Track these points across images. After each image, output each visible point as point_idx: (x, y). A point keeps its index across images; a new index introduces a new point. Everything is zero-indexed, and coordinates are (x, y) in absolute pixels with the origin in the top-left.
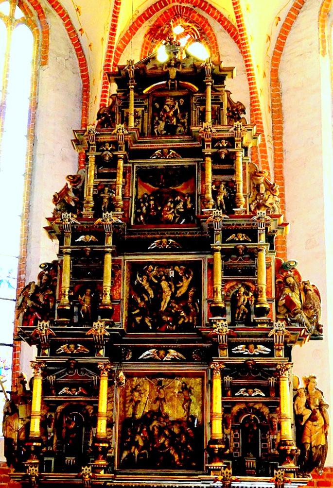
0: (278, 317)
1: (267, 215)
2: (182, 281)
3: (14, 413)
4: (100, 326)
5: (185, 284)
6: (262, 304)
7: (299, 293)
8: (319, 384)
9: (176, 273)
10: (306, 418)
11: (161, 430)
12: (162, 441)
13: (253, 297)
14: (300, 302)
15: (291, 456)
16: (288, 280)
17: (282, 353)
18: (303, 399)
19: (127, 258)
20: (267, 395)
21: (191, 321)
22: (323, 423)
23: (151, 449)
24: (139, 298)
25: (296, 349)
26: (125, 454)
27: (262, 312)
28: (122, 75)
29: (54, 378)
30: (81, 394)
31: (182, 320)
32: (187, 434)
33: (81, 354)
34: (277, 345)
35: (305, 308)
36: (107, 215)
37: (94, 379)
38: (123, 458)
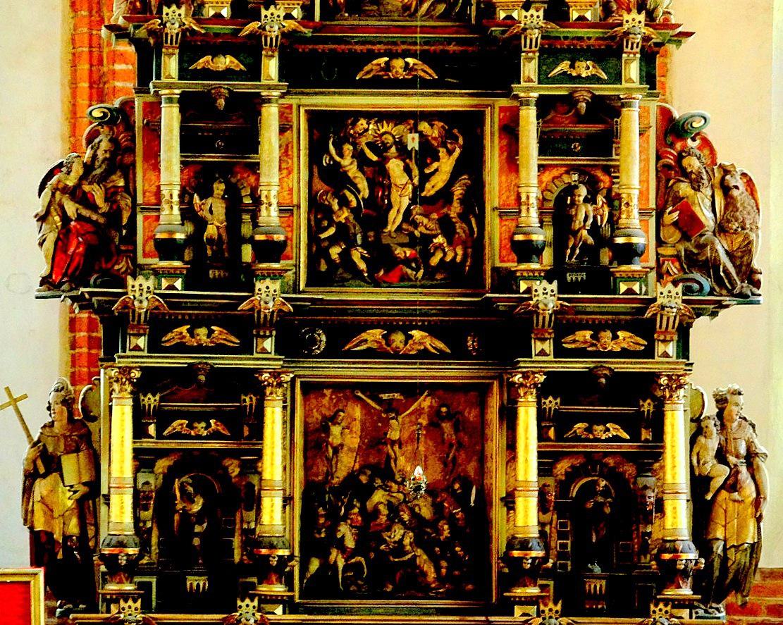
0: (661, 251)
1: (646, 25)
2: (437, 159)
3: (51, 473)
4: (272, 292)
5: (445, 165)
6: (629, 236)
7: (709, 193)
8: (745, 407)
9: (423, 138)
10: (717, 482)
11: (394, 509)
12: (398, 532)
13: (605, 206)
14: (711, 215)
15: (684, 573)
16: (685, 162)
17: (671, 349)
18: (712, 443)
19: (306, 100)
20: (635, 437)
21: (459, 259)
22: (754, 495)
23: (372, 555)
24: (336, 201)
25: (701, 328)
26: (315, 565)
27: (628, 253)
28: (642, 481)
29: (155, 400)
30: (215, 436)
31: (439, 255)
32: (451, 520)
33: (221, 349)
34: (662, 333)
35: (721, 229)
36: (272, 14)
37: (248, 403)
38: (308, 575)
